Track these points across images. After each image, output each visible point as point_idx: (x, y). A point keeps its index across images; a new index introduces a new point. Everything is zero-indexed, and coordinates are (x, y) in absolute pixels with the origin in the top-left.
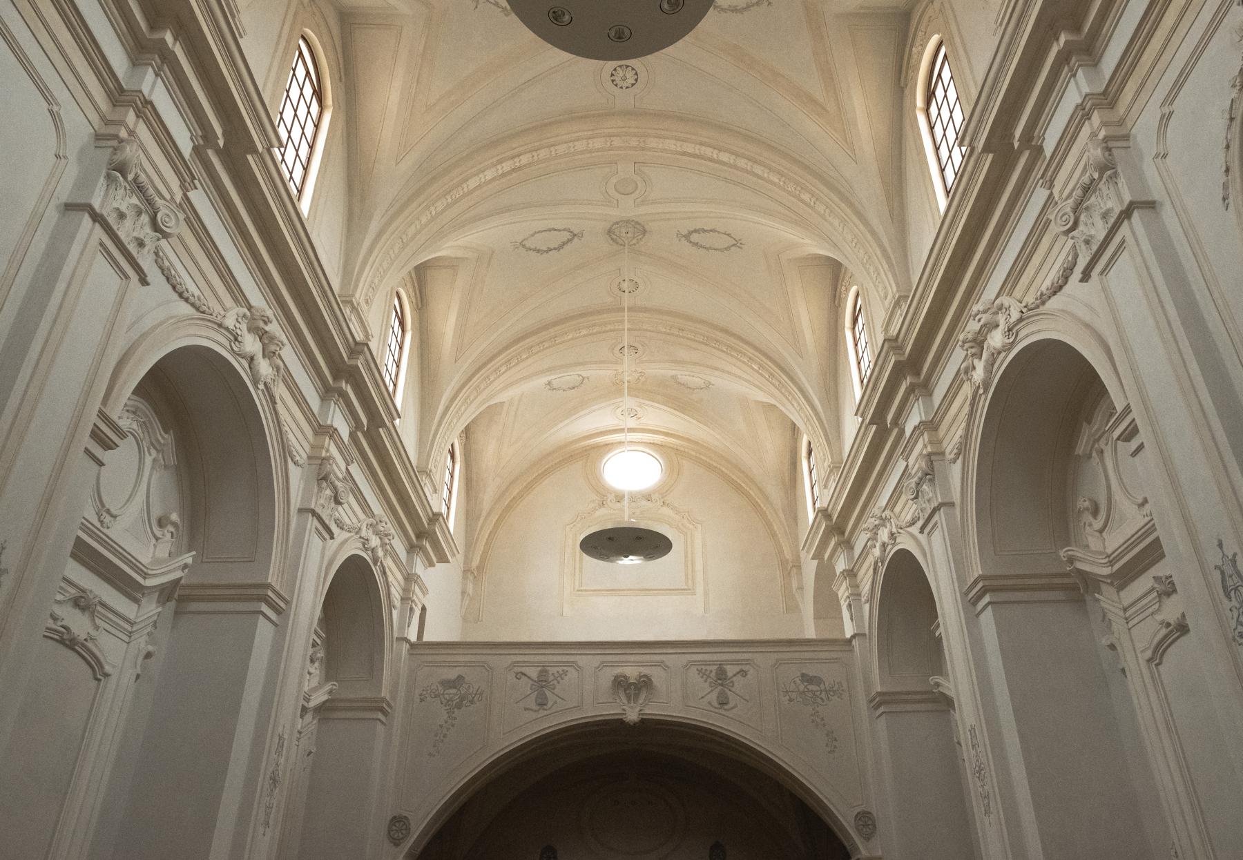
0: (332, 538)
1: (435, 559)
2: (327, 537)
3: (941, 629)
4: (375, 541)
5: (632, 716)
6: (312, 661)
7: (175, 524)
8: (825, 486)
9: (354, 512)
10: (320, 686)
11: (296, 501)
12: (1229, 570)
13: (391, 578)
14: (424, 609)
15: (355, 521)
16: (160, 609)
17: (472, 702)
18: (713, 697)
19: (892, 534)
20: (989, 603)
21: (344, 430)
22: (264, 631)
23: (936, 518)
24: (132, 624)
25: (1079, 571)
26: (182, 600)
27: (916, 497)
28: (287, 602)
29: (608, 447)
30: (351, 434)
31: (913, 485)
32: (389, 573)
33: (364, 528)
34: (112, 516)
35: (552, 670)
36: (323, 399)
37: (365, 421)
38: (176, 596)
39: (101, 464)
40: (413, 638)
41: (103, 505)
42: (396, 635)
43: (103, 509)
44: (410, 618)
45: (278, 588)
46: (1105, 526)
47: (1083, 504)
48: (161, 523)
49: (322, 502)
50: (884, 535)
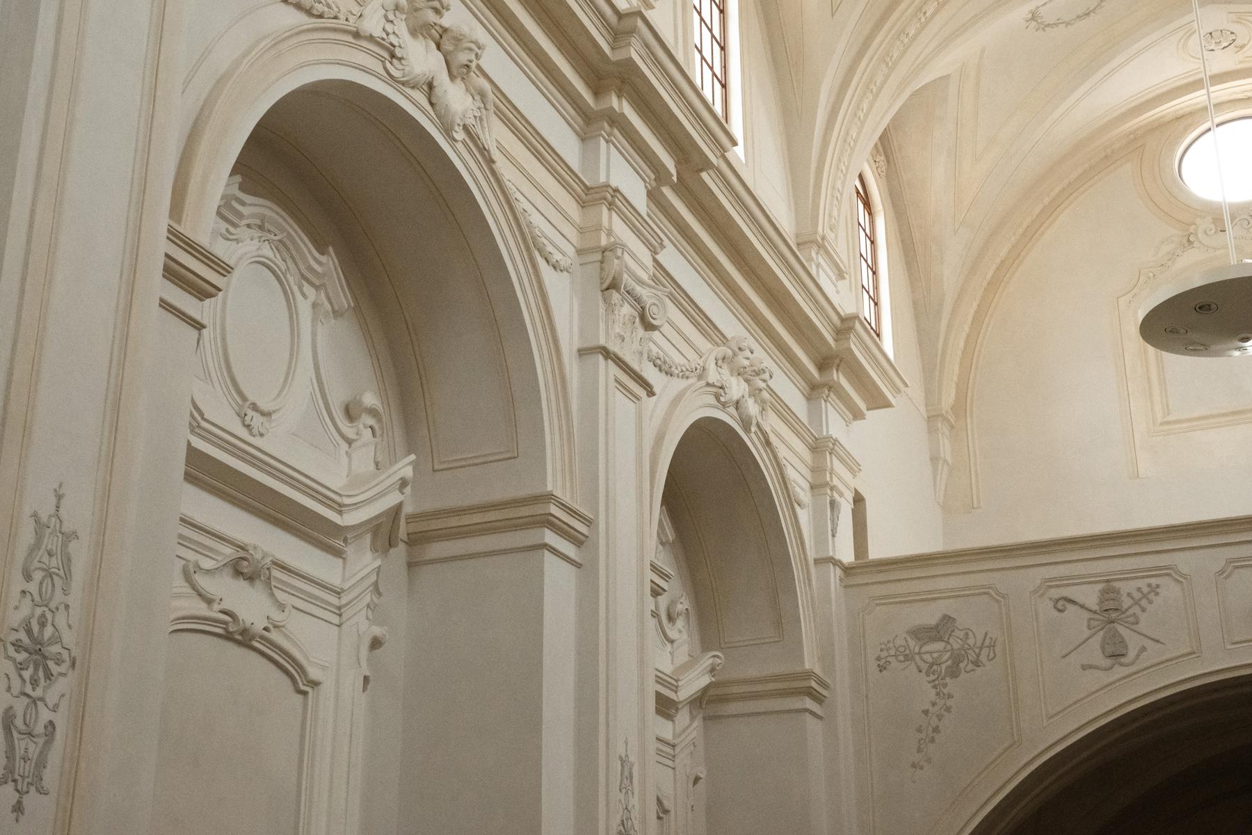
0: (651, 393)
1: (862, 405)
2: (641, 392)
4: (737, 388)
6: (671, 618)
7: (373, 412)
10: (693, 660)
11: (569, 341)
13: (782, 452)
14: (858, 500)
15: (691, 355)
16: (378, 563)
17: (977, 664)
21: (634, 188)
22: (558, 579)
24: (338, 594)
26: (415, 541)
28: (588, 522)
29: (1185, 120)
30: (650, 195)
32: (773, 438)
33: (711, 366)
34: (263, 414)
35: (1125, 587)
36: (583, 138)
37: (669, 163)
38: (403, 532)
39: (199, 326)
40: (846, 554)
41: (244, 399)
42: (811, 554)
43: (246, 408)
45: (567, 500)
48: (350, 413)
49: (617, 329)
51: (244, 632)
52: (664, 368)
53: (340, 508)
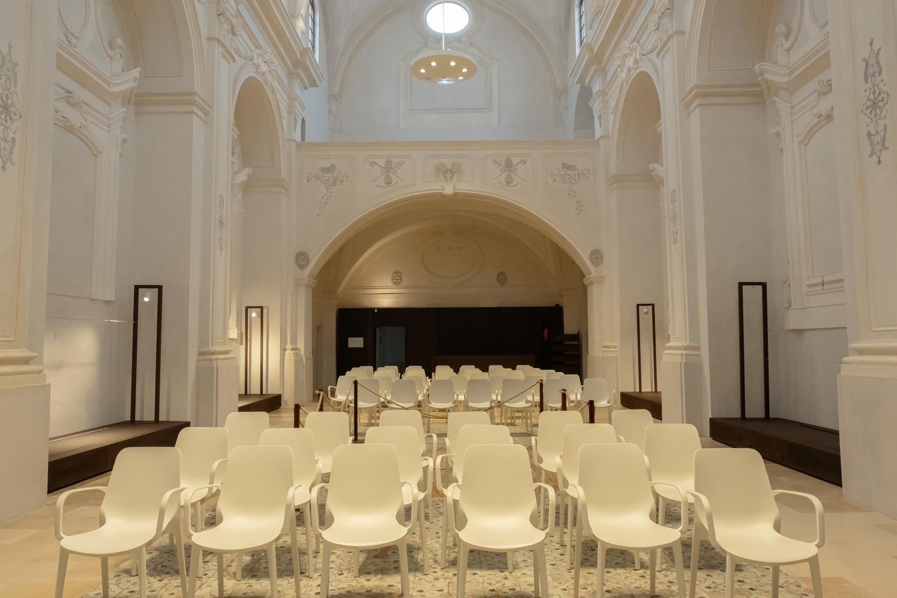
0: (234, 61)
3: (662, 127)
4: (264, 68)
5: (449, 190)
6: (111, 47)
8: (591, 28)
9: (247, 45)
12: (872, 61)
13: (279, 96)
14: (303, 121)
17: (342, 182)
18: (503, 178)
19: (636, 60)
20: (699, 105)
22: (198, 126)
23: (670, 44)
25: (766, 81)
27: (657, 29)
28: (210, 107)
31: (656, 19)
33: (255, 57)
34: (76, 38)
41: (68, 30)
44: (295, 126)
46: (792, 46)
47: (781, 29)
50: (630, 62)
51: (72, 127)
52: (237, 52)
53: (109, 84)
